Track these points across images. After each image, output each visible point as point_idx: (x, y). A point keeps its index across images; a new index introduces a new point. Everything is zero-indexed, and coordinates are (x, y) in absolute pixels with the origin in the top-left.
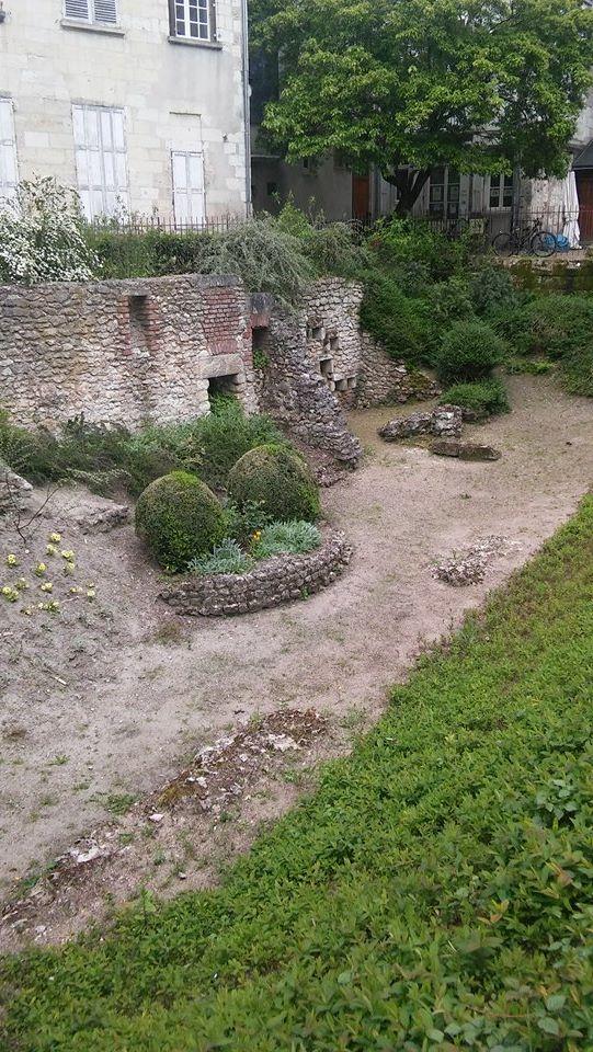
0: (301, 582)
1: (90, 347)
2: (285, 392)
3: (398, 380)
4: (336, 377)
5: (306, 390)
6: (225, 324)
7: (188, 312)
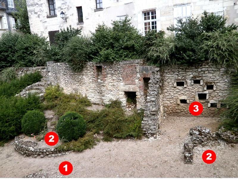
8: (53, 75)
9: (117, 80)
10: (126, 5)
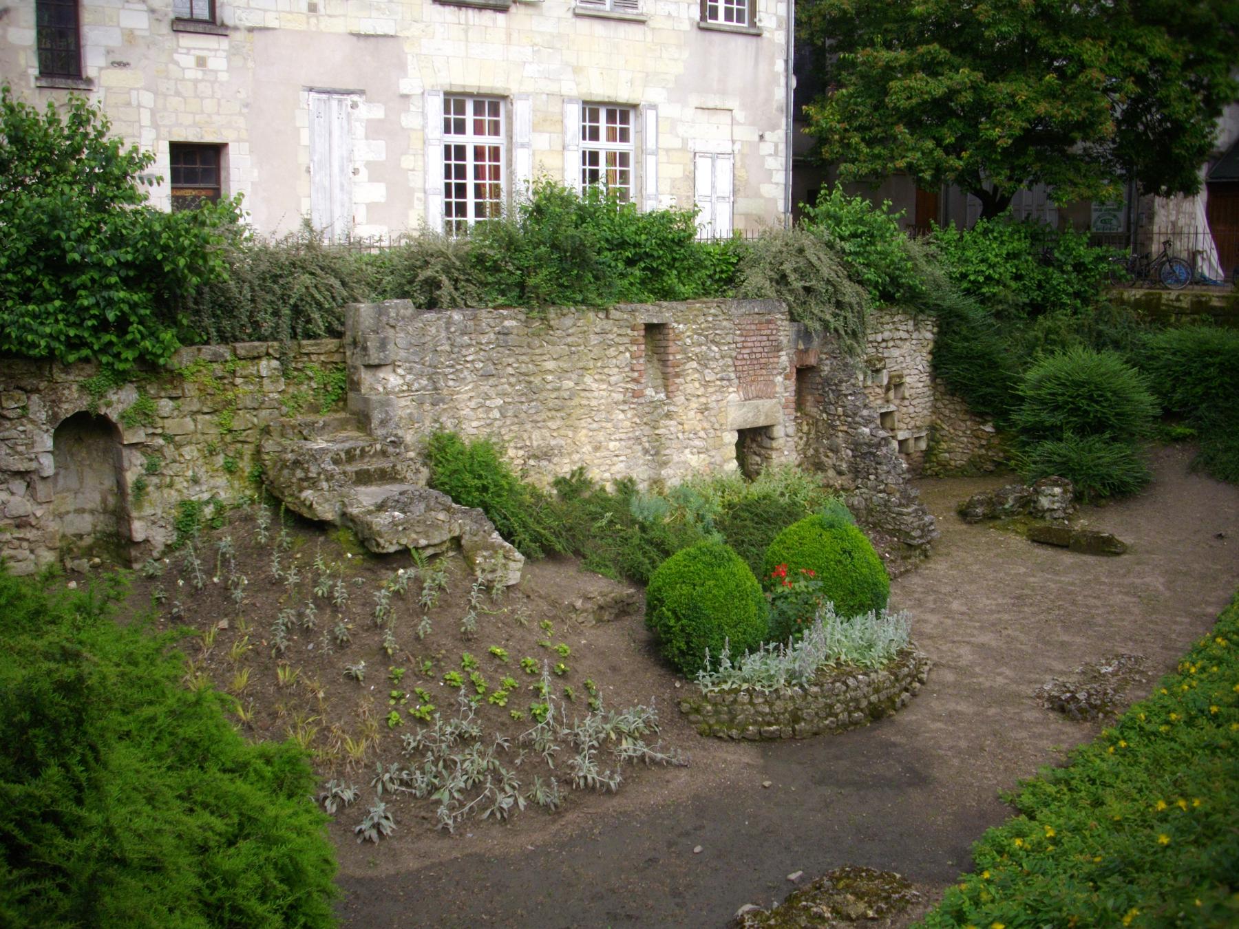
0: (864, 704)
1: (595, 386)
2: (835, 451)
3: (984, 442)
4: (901, 435)
5: (865, 449)
6: (763, 361)
7: (717, 344)
8: (416, 386)
9: (718, 383)
10: (362, 43)
